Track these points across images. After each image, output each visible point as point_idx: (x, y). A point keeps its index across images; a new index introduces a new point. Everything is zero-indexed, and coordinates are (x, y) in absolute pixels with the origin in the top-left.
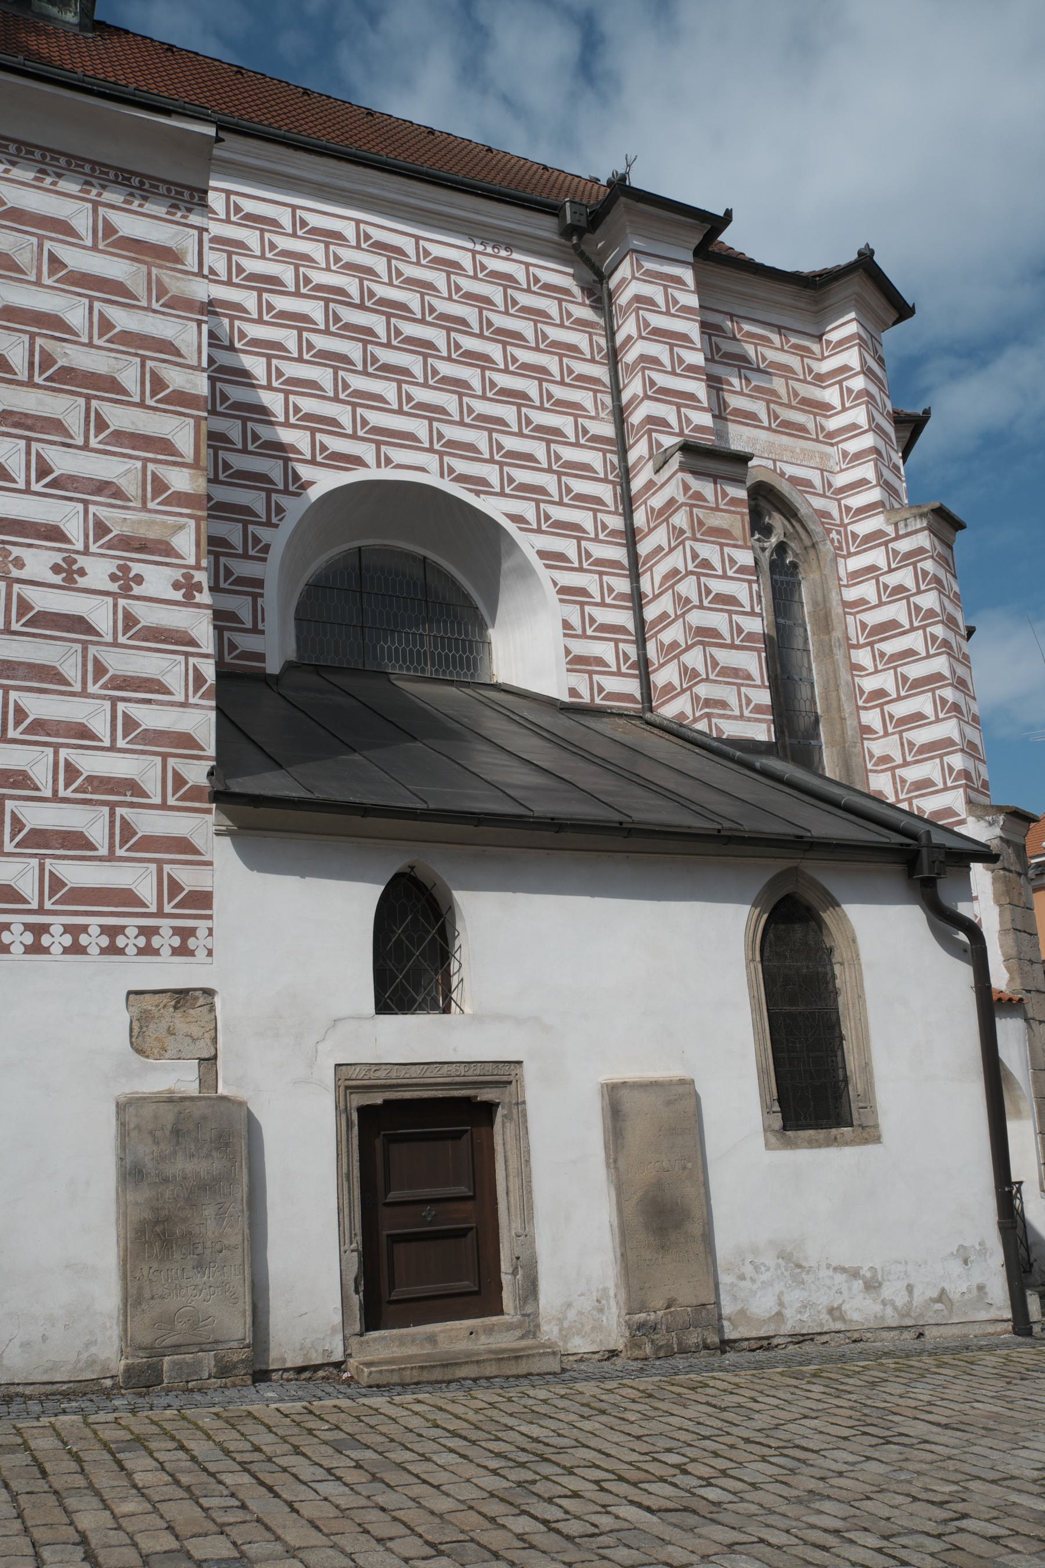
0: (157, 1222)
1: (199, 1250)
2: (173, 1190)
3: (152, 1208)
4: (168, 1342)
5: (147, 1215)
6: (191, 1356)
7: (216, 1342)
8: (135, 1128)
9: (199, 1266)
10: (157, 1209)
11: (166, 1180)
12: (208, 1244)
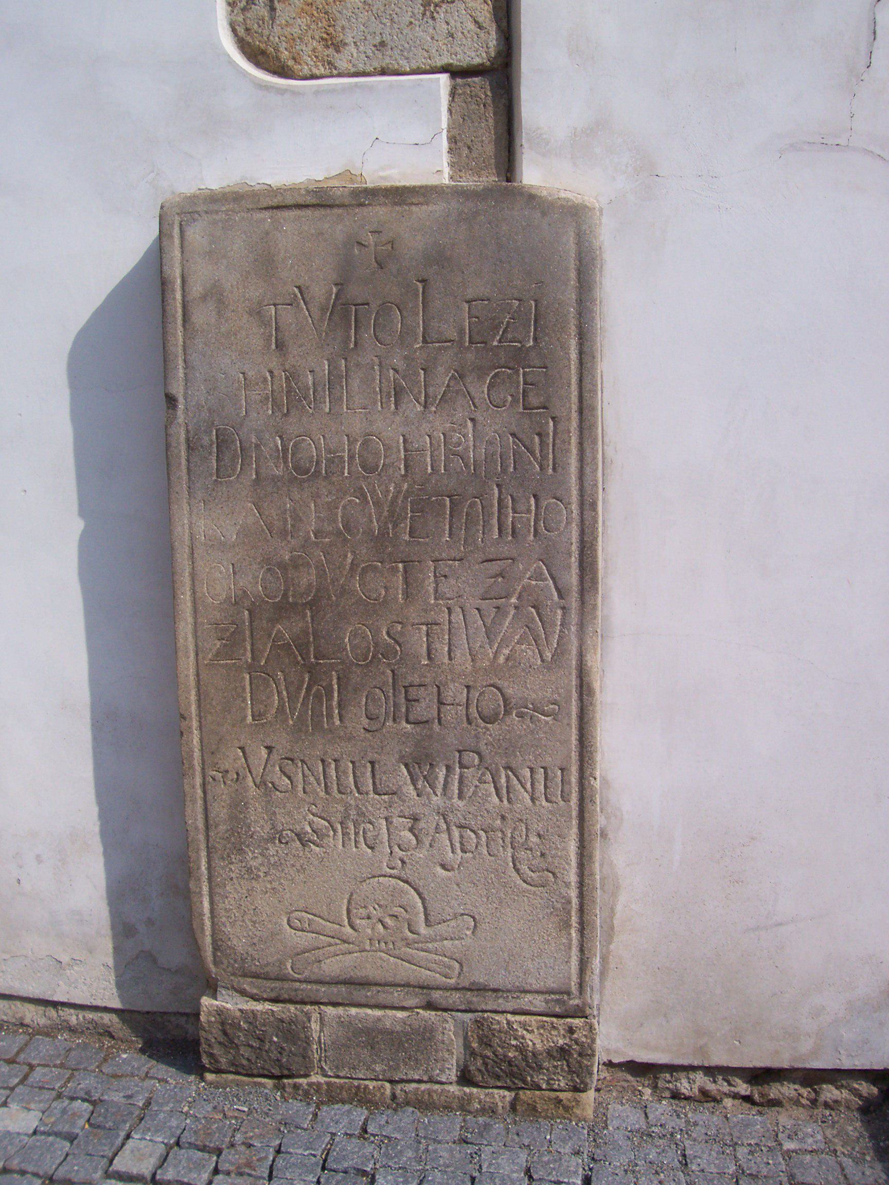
0: (284, 609)
1: (425, 708)
2: (331, 507)
3: (269, 563)
4: (332, 967)
5: (253, 581)
6: (400, 1014)
7: (479, 989)
8: (204, 298)
9: (420, 762)
10: (283, 566)
11: (303, 473)
12: (455, 692)
